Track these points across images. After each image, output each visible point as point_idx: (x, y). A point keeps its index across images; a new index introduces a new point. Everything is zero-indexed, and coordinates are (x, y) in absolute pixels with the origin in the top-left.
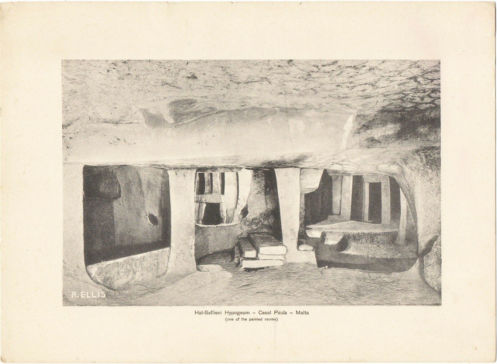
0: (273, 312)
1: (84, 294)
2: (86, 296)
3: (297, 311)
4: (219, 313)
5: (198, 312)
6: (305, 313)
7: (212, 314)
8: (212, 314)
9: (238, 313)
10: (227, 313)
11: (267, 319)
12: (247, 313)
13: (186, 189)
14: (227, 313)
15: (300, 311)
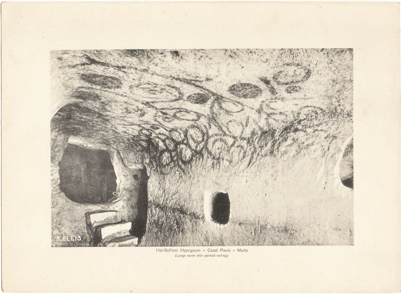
0: (219, 250)
1: (65, 239)
2: (66, 239)
3: (238, 249)
4: (176, 250)
5: (183, 250)
6: (244, 250)
7: (170, 251)
8: (170, 251)
9: (191, 250)
10: (182, 251)
11: (189, 256)
12: (198, 250)
13: (265, 240)
14: (182, 251)
15: (240, 249)
